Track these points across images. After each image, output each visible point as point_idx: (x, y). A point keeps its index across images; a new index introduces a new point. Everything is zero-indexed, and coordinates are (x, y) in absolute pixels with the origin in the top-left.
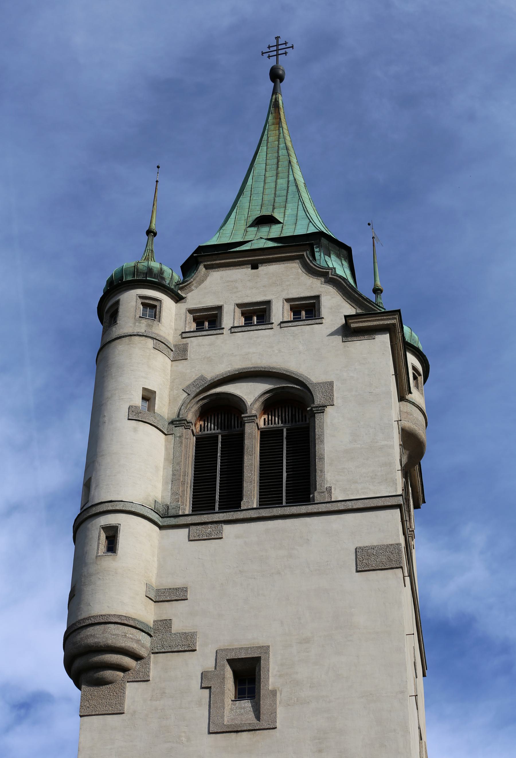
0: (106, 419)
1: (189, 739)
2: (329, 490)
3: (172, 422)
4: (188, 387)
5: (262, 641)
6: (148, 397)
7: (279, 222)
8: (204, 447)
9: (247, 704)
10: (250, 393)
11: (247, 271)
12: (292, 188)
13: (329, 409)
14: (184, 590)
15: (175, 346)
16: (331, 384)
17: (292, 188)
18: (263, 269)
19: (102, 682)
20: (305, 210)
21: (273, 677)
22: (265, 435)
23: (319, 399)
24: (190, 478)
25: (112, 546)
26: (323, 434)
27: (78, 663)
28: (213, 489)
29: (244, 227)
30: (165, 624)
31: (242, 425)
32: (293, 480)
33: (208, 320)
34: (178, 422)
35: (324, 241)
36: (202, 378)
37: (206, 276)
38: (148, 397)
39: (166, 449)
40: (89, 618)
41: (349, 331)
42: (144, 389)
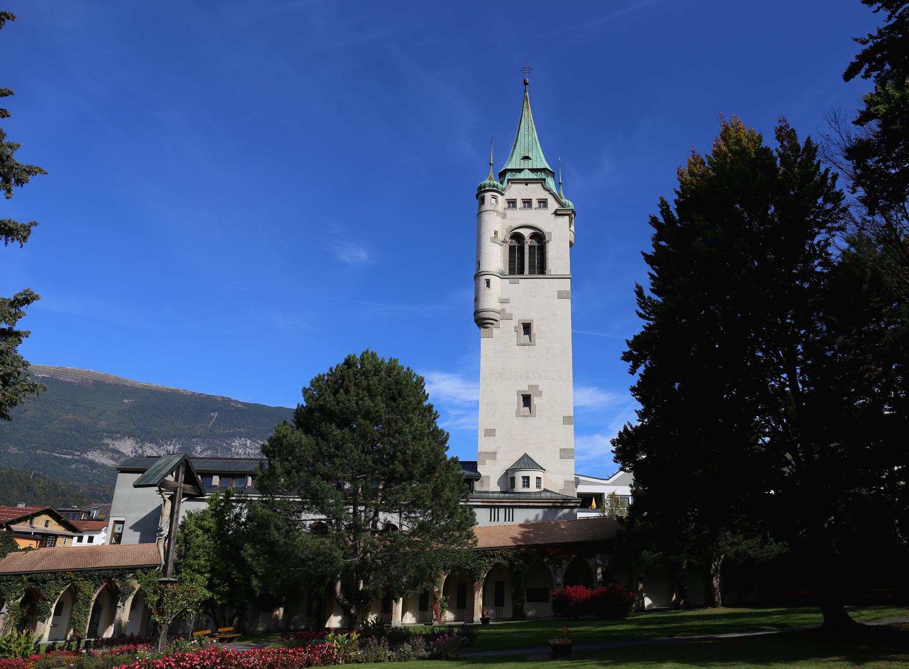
6: (496, 233)
8: (512, 249)
9: (527, 336)
10: (526, 233)
11: (524, 185)
19: (487, 328)
21: (534, 329)
23: (547, 239)
25: (488, 285)
28: (516, 267)
30: (503, 310)
32: (540, 268)
33: (512, 203)
38: (496, 233)
41: (556, 213)
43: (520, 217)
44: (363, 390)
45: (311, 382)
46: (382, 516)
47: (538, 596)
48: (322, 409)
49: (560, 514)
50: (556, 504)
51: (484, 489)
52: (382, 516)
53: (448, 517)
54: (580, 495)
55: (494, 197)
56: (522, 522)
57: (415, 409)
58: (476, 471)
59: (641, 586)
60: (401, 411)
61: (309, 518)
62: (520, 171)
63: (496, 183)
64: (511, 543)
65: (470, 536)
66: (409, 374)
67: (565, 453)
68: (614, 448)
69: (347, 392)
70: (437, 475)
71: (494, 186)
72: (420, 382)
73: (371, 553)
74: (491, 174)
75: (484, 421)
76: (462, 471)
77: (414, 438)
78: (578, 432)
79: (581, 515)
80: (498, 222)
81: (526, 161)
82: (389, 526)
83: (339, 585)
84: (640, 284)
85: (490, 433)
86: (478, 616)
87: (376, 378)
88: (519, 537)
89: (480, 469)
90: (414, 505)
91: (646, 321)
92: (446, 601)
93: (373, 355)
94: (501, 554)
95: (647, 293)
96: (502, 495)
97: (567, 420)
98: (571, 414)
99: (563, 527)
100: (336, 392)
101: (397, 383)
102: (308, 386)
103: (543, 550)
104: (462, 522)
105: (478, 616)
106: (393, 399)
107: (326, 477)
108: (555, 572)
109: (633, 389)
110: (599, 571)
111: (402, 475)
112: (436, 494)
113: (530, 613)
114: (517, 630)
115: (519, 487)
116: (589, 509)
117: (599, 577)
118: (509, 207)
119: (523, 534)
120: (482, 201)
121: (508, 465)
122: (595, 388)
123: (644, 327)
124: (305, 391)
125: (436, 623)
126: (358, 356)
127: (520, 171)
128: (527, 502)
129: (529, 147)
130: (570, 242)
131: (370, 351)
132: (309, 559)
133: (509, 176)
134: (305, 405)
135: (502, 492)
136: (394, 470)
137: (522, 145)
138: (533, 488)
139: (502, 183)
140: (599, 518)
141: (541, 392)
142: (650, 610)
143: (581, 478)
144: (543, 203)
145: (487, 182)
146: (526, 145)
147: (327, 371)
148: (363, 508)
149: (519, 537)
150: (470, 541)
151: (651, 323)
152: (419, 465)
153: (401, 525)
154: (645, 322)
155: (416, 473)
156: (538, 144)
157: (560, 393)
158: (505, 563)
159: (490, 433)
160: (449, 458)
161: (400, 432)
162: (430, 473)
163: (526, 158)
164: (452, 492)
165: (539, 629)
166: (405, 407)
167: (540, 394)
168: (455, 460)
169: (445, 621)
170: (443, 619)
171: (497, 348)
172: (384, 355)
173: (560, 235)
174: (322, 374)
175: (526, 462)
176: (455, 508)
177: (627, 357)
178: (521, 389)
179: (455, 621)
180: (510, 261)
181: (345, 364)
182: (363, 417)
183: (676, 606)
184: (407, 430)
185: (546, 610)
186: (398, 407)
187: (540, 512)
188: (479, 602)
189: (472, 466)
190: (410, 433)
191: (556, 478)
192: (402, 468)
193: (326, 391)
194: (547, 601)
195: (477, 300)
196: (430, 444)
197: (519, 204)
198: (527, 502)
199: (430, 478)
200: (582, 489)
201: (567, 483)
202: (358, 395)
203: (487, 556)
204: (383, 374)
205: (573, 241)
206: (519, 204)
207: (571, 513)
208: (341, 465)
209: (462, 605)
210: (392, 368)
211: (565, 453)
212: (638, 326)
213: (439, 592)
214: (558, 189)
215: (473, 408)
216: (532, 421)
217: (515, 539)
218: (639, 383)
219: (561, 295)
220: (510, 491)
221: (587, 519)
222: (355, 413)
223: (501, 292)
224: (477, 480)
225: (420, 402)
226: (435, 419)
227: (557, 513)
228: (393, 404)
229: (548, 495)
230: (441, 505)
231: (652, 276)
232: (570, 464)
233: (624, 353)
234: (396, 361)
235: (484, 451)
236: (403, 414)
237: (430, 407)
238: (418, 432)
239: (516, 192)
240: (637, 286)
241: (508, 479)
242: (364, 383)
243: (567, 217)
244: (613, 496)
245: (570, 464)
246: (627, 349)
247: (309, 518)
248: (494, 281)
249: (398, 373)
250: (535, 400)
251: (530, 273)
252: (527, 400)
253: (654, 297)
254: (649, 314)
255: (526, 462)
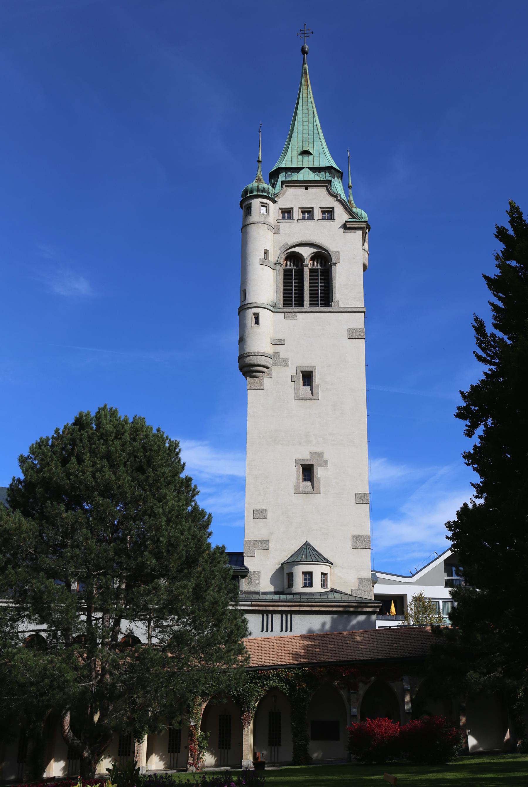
0: (251, 263)
1: (288, 402)
2: (338, 302)
3: (275, 264)
4: (281, 247)
5: (313, 364)
7: (311, 154)
8: (287, 273)
9: (308, 389)
10: (306, 252)
11: (303, 190)
12: (316, 131)
13: (337, 264)
14: (284, 340)
15: (275, 226)
16: (339, 252)
17: (316, 131)
18: (310, 189)
20: (323, 147)
21: (317, 379)
22: (311, 271)
23: (334, 260)
24: (282, 290)
25: (257, 321)
26: (335, 276)
27: (246, 369)
28: (292, 297)
29: (296, 155)
30: (277, 354)
31: (303, 267)
33: (287, 213)
34: (277, 264)
35: (333, 170)
36: (286, 244)
37: (286, 191)
38: (266, 252)
39: (273, 276)
40: (250, 353)
41: (346, 227)
42: (265, 250)
43: (298, 232)
44: (102, 458)
45: (31, 448)
46: (124, 624)
47: (327, 731)
48: (46, 483)
49: (354, 622)
50: (349, 608)
51: (253, 589)
52: (124, 624)
53: (214, 625)
54: (378, 597)
55: (264, 205)
56: (304, 632)
57: (169, 483)
58: (242, 565)
59: (463, 720)
60: (151, 486)
61: (26, 627)
62: (297, 170)
63: (266, 186)
64: (290, 660)
65: (241, 650)
66: (160, 437)
67: (359, 542)
68: (450, 534)
69: (80, 461)
70: (199, 569)
71: (264, 190)
72: (173, 450)
73: (111, 674)
74: (260, 175)
75: (252, 501)
76: (228, 566)
77: (169, 521)
78: (376, 515)
79: (380, 624)
80: (268, 239)
81: (306, 158)
82: (132, 640)
83: (68, 719)
84: (481, 317)
85: (260, 514)
86: (248, 761)
87: (117, 443)
88: (302, 652)
89: (248, 562)
90: (171, 607)
91: (488, 366)
92: (205, 738)
93: (113, 413)
94: (278, 676)
95: (490, 329)
96: (277, 597)
97: (360, 498)
98: (366, 490)
99: (358, 639)
100: (64, 462)
101: (144, 448)
102: (26, 453)
103: (333, 669)
104: (232, 632)
105: (248, 761)
106: (140, 469)
107: (52, 574)
108: (349, 699)
109: (467, 456)
110: (407, 698)
111: (153, 570)
112: (198, 595)
113: (315, 755)
114: (307, 778)
115: (299, 586)
116: (387, 616)
117: (408, 707)
118: (283, 218)
119: (306, 648)
120: (248, 210)
121: (284, 557)
122: (384, 460)
123: (485, 373)
124: (22, 460)
125: (192, 769)
126: (93, 414)
127: (297, 170)
128: (309, 606)
129: (309, 139)
130: (364, 265)
131: (108, 407)
132: (32, 684)
133: (282, 177)
134: (22, 478)
135: (276, 593)
136: (143, 564)
137: (300, 135)
138: (317, 587)
139: (273, 186)
140: (399, 629)
141: (326, 461)
142: (476, 753)
143: (379, 575)
144: (328, 213)
145: (255, 184)
146: (306, 136)
147: (51, 433)
148: (99, 615)
149: (302, 652)
150: (240, 658)
151: (494, 368)
152: (176, 556)
153: (150, 637)
154: (486, 368)
155: (173, 567)
156: (321, 135)
157: (350, 464)
158: (282, 686)
159: (260, 514)
160: (213, 546)
161: (152, 514)
162: (190, 567)
163: (305, 153)
164: (218, 592)
165: (336, 777)
166: (157, 481)
167: (325, 464)
168: (221, 550)
169: (204, 767)
170: (201, 763)
171: (268, 403)
172: (127, 412)
173: (350, 255)
174: (44, 437)
175: (308, 553)
176: (224, 613)
177: (462, 414)
178: (299, 456)
179: (216, 766)
180: (285, 290)
181: (75, 424)
182: (102, 495)
183: (509, 748)
184: (161, 510)
185: (338, 750)
186: (147, 480)
187: (327, 619)
188: (248, 739)
189: (238, 558)
190: (164, 514)
191: (347, 574)
192: (154, 561)
193: (52, 459)
194: (337, 738)
195: (242, 340)
196: (189, 529)
197: (297, 214)
198: (309, 606)
199: (190, 573)
200: (380, 589)
201: (361, 581)
202: (94, 465)
203: (259, 678)
204: (127, 437)
205: (367, 263)
206: (297, 214)
207: (368, 621)
208: (72, 557)
209: (226, 743)
210: (138, 428)
211: (359, 542)
212: (476, 373)
213: (196, 727)
214: (347, 194)
215: (237, 485)
216: (315, 499)
217: (295, 655)
218: (476, 448)
219: (351, 335)
220: (287, 591)
221: (390, 629)
222: (89, 488)
223: (271, 331)
224: (244, 576)
225: (176, 474)
226: (193, 496)
227: (350, 621)
228: (141, 477)
229: (338, 596)
230: (205, 610)
231: (495, 308)
232: (365, 556)
233: (459, 408)
234: (143, 420)
235: (252, 538)
236: (154, 490)
237: (189, 480)
238: (174, 513)
239: (293, 198)
240: (477, 320)
241: (284, 575)
242: (103, 449)
243: (360, 232)
244: (419, 599)
245: (365, 556)
246: (463, 404)
247: (26, 627)
248: (265, 316)
249: (147, 436)
250: (319, 472)
251: (312, 305)
252: (308, 472)
253: (499, 334)
254: (492, 357)
255: (308, 553)
